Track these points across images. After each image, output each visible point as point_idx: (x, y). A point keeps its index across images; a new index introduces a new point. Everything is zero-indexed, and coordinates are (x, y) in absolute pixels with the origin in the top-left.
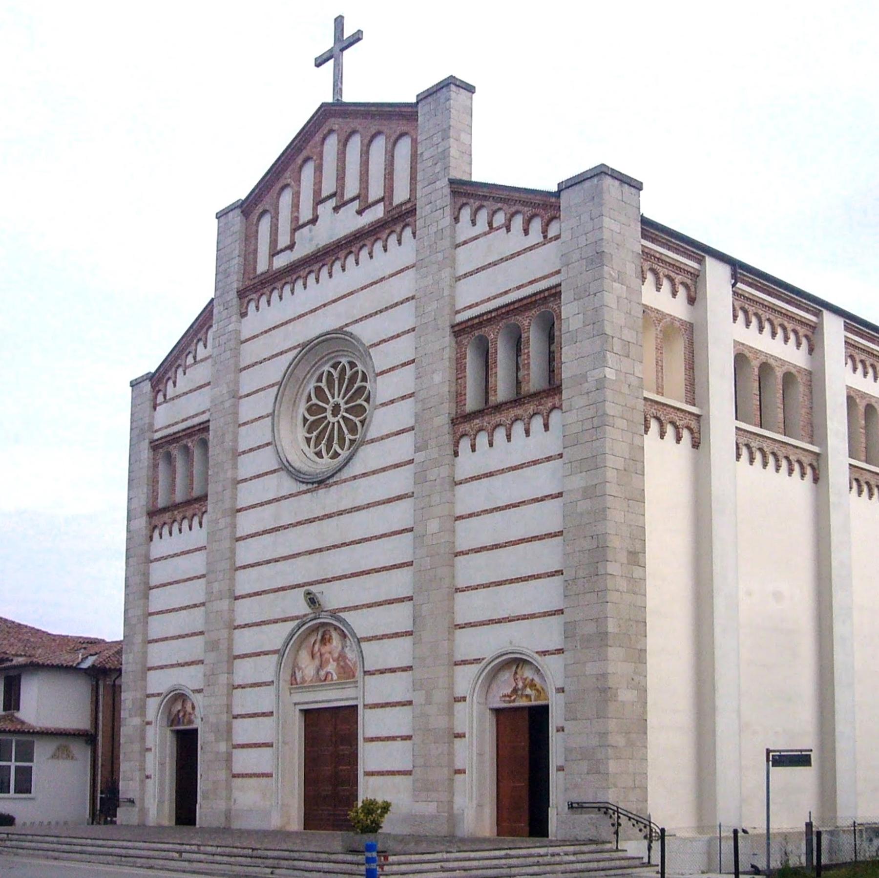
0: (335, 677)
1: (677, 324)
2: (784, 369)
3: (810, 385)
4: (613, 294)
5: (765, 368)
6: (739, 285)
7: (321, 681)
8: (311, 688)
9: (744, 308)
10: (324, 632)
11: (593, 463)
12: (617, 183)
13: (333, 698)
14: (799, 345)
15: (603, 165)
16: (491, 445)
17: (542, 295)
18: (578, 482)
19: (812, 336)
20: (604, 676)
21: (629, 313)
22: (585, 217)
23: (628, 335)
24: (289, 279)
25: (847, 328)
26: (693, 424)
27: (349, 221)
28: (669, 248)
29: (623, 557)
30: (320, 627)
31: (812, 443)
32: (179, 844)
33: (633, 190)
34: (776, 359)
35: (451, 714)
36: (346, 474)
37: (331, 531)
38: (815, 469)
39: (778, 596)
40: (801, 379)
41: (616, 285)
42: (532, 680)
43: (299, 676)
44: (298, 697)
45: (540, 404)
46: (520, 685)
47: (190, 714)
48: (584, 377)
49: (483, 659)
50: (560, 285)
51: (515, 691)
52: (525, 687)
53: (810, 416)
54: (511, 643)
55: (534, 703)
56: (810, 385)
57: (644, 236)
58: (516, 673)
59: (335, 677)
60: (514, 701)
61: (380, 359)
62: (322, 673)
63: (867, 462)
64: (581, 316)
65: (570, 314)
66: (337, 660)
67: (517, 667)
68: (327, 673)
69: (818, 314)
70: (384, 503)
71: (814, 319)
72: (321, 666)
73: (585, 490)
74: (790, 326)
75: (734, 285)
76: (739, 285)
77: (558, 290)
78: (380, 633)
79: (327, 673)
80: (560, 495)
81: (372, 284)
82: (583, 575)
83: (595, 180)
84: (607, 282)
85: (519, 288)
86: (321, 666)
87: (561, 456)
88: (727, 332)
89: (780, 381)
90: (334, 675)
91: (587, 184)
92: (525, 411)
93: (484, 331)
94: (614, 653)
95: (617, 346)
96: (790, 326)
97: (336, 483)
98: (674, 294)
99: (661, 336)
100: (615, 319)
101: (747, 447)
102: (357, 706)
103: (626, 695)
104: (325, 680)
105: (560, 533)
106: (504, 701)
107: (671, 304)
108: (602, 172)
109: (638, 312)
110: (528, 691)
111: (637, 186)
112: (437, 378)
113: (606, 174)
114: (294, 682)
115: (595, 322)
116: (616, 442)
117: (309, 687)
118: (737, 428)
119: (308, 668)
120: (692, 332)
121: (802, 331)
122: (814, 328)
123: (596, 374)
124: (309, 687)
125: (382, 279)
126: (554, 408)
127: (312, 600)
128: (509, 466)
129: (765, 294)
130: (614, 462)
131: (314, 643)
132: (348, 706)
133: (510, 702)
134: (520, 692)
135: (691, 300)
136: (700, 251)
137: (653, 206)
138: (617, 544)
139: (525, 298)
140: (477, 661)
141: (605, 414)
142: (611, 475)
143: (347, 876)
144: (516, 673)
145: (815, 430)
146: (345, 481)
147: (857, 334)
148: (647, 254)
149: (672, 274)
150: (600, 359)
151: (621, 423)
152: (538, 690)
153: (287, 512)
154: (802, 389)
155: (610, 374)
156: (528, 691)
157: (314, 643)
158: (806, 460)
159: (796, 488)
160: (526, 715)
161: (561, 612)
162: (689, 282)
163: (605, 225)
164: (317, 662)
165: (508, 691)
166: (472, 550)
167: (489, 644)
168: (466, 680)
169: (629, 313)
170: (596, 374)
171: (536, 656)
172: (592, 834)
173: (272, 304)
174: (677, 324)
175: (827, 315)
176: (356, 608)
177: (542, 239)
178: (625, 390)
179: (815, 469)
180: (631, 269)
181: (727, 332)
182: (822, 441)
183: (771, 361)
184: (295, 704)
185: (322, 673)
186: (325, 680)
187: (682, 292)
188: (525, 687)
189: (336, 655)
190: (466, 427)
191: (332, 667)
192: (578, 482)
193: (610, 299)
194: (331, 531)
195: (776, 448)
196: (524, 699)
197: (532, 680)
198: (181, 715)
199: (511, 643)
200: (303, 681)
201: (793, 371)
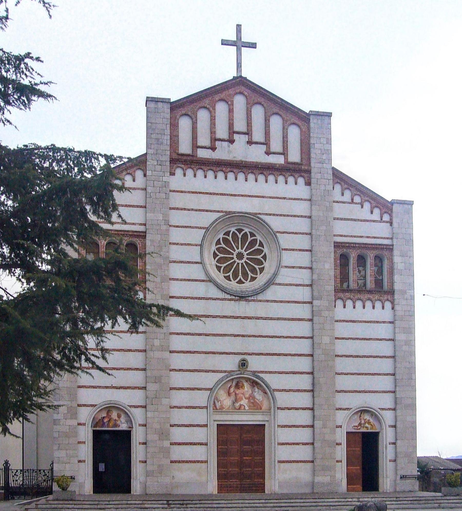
0: (247, 408)
7: (236, 409)
8: (227, 412)
10: (238, 382)
13: (245, 419)
16: (354, 307)
17: (382, 247)
24: (214, 168)
27: (257, 155)
30: (243, 378)
32: (257, 507)
35: (334, 433)
36: (260, 297)
37: (250, 327)
42: (369, 420)
43: (218, 405)
44: (218, 417)
45: (381, 296)
46: (363, 422)
47: (115, 420)
49: (351, 409)
51: (360, 424)
52: (365, 423)
54: (366, 402)
55: (369, 431)
58: (360, 416)
59: (247, 408)
60: (360, 429)
61: (196, 236)
62: (237, 405)
64: (403, 264)
66: (248, 398)
67: (361, 414)
68: (241, 405)
70: (289, 320)
72: (236, 400)
78: (287, 388)
79: (241, 405)
81: (235, 195)
82: (405, 378)
85: (368, 237)
86: (236, 400)
90: (246, 406)
92: (373, 297)
93: (365, 252)
97: (254, 300)
102: (265, 425)
104: (239, 409)
106: (355, 429)
110: (367, 425)
112: (327, 266)
114: (215, 408)
117: (224, 412)
119: (226, 402)
124: (224, 412)
125: (284, 198)
127: (243, 364)
128: (364, 320)
131: (230, 388)
132: (234, 425)
133: (357, 429)
134: (362, 425)
139: (136, 232)
140: (347, 409)
143: (81, 510)
144: (360, 416)
146: (260, 301)
152: (371, 425)
153: (215, 308)
156: (367, 425)
157: (230, 388)
160: (360, 435)
164: (233, 397)
165: (357, 424)
166: (345, 355)
167: (356, 402)
168: (341, 417)
171: (379, 410)
172: (411, 488)
173: (217, 177)
176: (270, 372)
177: (380, 220)
184: (215, 421)
185: (237, 405)
186: (239, 409)
188: (365, 423)
189: (247, 396)
190: (342, 295)
191: (244, 402)
194: (250, 327)
196: (365, 428)
197: (369, 420)
198: (106, 420)
199: (366, 402)
200: (222, 408)
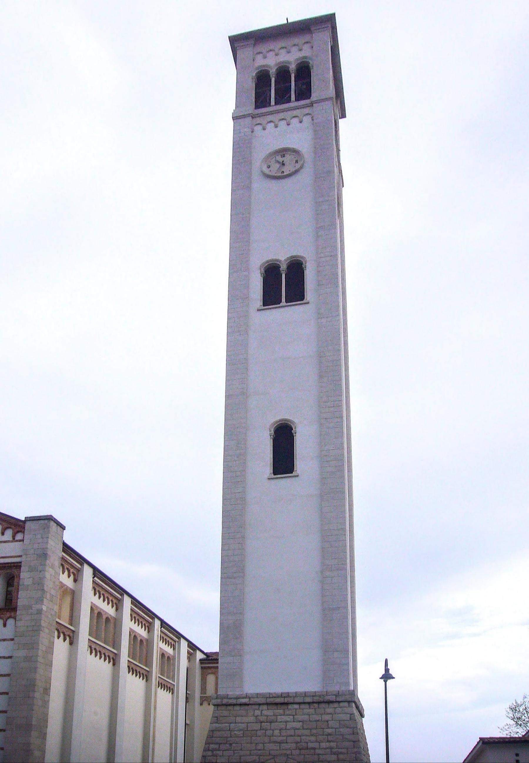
1: (69, 590)
2: (106, 616)
3: (115, 624)
4: (49, 573)
5: (99, 614)
6: (95, 578)
9: (97, 589)
11: (33, 646)
12: (55, 524)
14: (113, 607)
15: (51, 516)
18: (21, 653)
19: (118, 605)
20: (29, 744)
21: (54, 582)
22: (39, 536)
23: (53, 592)
25: (95, 575)
26: (71, 635)
28: (70, 557)
29: (41, 690)
31: (114, 648)
33: (62, 529)
34: (104, 611)
38: (114, 660)
39: (96, 713)
40: (112, 621)
41: (51, 569)
48: (31, 607)
50: (21, 562)
53: (10, 589)
56: (115, 624)
57: (64, 551)
63: (139, 663)
65: (25, 577)
69: (122, 595)
71: (80, 566)
73: (26, 657)
74: (111, 598)
75: (93, 578)
76: (95, 578)
77: (20, 564)
80: (10, 657)
83: (46, 521)
84: (47, 568)
87: (12, 640)
88: (89, 598)
89: (104, 620)
91: (42, 522)
94: (34, 734)
95: (48, 596)
96: (111, 598)
98: (69, 576)
99: (62, 593)
100: (49, 585)
101: (93, 649)
103: (37, 753)
105: (8, 675)
107: (67, 581)
108: (50, 518)
109: (57, 583)
111: (63, 528)
113: (52, 520)
115: (39, 584)
116: (43, 638)
118: (89, 639)
120: (74, 594)
121: (115, 601)
122: (79, 571)
123: (38, 606)
126: (10, 617)
129: (144, 614)
130: (42, 648)
135: (75, 581)
136: (123, 591)
137: (69, 538)
138: (40, 684)
141: (40, 625)
142: (40, 653)
145: (116, 643)
147: (136, 606)
148: (63, 558)
149: (70, 568)
150: (40, 600)
151: (47, 631)
154: (112, 625)
155: (44, 608)
158: (111, 656)
159: (106, 667)
161: (5, 712)
162: (75, 572)
163: (49, 542)
169: (54, 582)
170: (38, 606)
174: (69, 590)
175: (126, 596)
178: (50, 616)
179: (114, 660)
180: (57, 563)
181: (89, 598)
182: (119, 648)
183: (101, 611)
187: (72, 576)
192: (21, 653)
193: (48, 575)
195: (101, 649)
201: (110, 617)
